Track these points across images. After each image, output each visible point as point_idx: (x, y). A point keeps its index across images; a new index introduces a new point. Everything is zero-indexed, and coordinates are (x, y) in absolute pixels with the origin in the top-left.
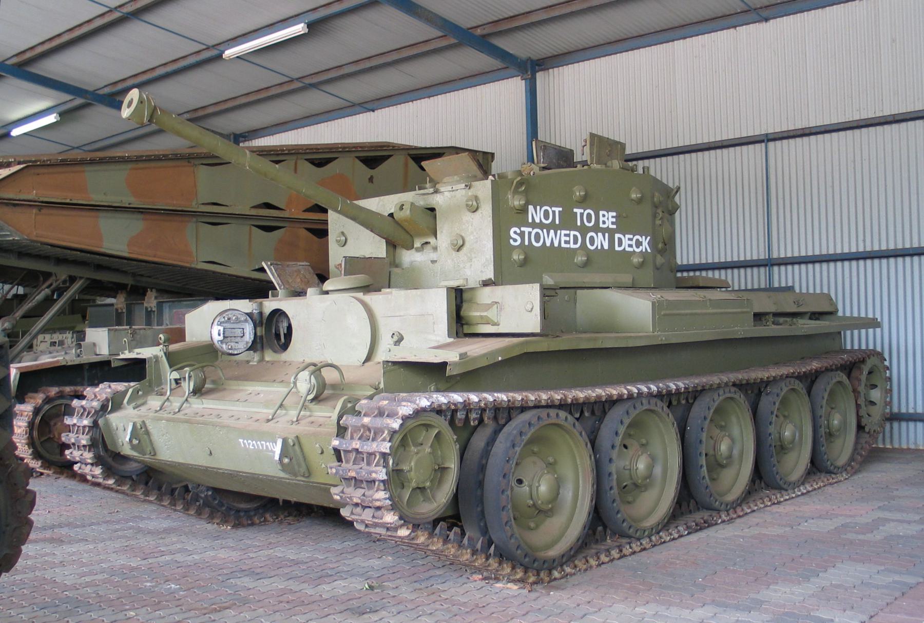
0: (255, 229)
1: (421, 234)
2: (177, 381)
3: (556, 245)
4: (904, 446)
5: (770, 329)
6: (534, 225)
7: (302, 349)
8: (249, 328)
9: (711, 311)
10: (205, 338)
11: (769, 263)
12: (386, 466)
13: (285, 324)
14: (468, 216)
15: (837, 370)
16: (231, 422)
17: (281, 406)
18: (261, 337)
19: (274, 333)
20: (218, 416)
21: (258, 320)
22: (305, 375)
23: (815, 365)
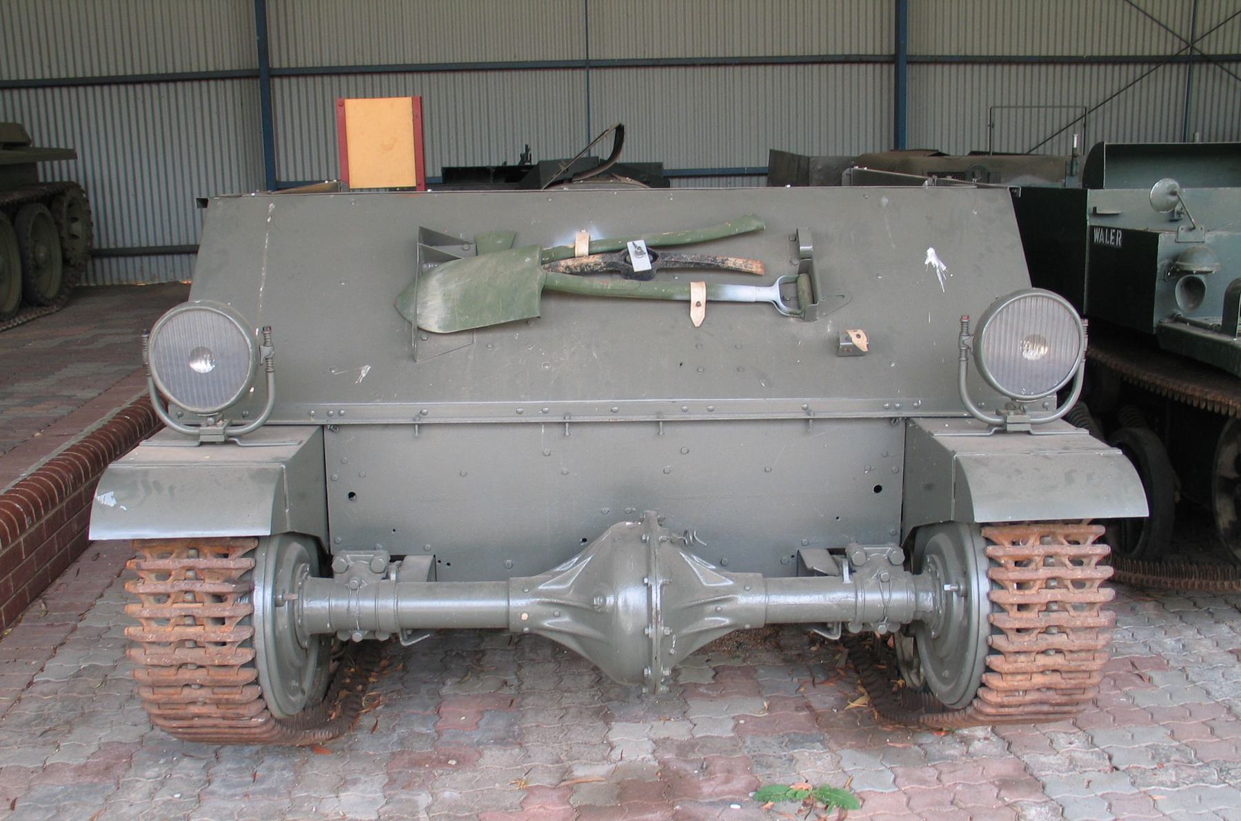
4: (108, 283)
15: (37, 201)
23: (17, 196)
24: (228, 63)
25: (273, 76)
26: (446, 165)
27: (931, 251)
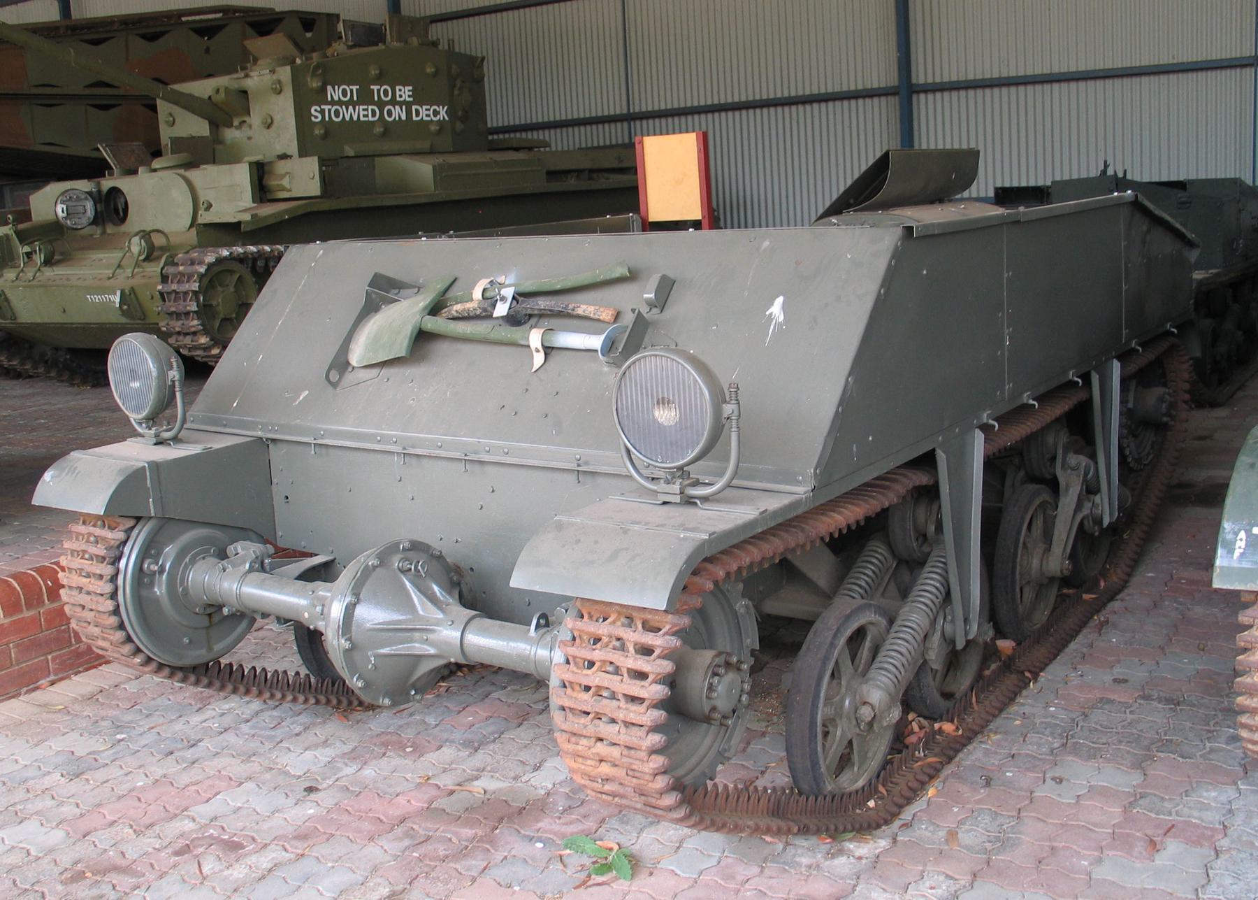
0: (90, 109)
1: (238, 115)
2: (29, 255)
3: (355, 118)
5: (556, 186)
6: (333, 103)
7: (136, 221)
8: (89, 205)
9: (496, 170)
10: (51, 217)
12: (198, 301)
13: (122, 200)
14: (274, 98)
16: (79, 283)
17: (119, 266)
18: (102, 212)
19: (112, 209)
20: (68, 279)
21: (97, 197)
22: (136, 240)
24: (875, 83)
25: (918, 92)
26: (999, 185)
27: (780, 300)
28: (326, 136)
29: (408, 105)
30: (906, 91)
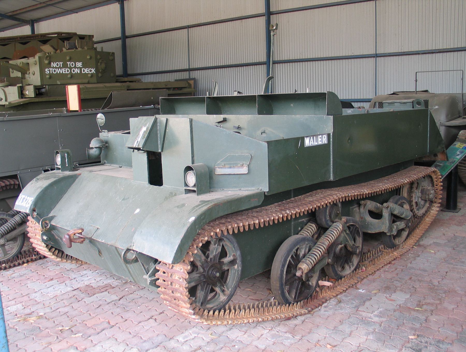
3: (61, 72)
6: (53, 68)
9: (106, 89)
11: (190, 70)
28: (50, 77)
29: (81, 69)
30: (269, 63)
